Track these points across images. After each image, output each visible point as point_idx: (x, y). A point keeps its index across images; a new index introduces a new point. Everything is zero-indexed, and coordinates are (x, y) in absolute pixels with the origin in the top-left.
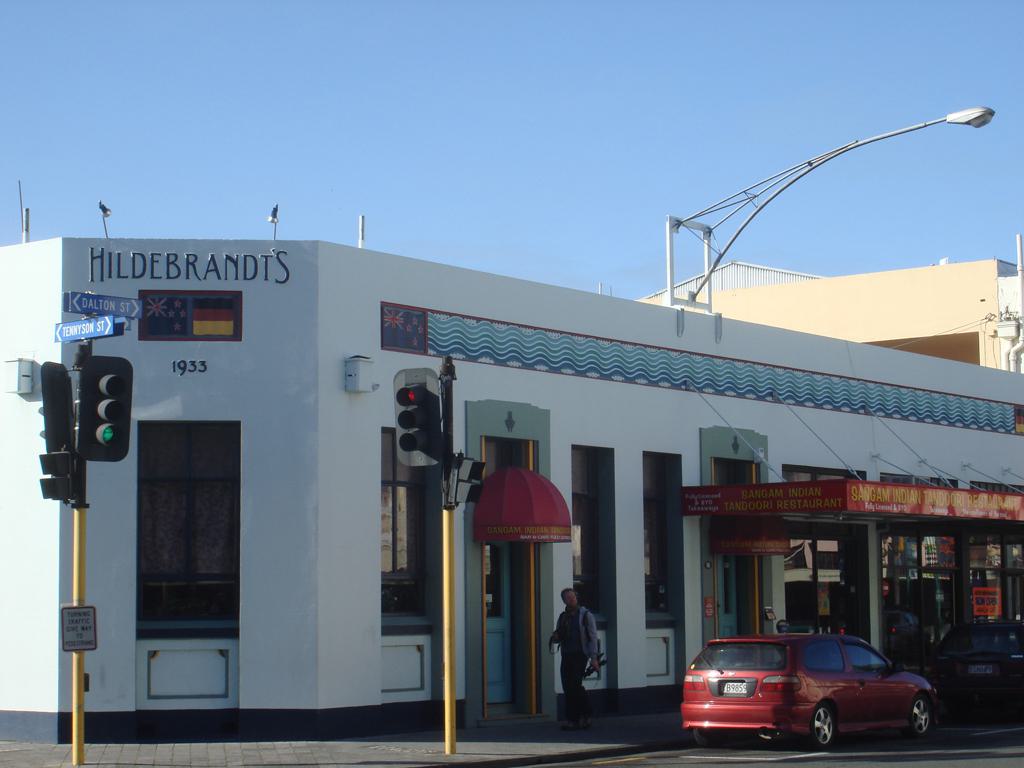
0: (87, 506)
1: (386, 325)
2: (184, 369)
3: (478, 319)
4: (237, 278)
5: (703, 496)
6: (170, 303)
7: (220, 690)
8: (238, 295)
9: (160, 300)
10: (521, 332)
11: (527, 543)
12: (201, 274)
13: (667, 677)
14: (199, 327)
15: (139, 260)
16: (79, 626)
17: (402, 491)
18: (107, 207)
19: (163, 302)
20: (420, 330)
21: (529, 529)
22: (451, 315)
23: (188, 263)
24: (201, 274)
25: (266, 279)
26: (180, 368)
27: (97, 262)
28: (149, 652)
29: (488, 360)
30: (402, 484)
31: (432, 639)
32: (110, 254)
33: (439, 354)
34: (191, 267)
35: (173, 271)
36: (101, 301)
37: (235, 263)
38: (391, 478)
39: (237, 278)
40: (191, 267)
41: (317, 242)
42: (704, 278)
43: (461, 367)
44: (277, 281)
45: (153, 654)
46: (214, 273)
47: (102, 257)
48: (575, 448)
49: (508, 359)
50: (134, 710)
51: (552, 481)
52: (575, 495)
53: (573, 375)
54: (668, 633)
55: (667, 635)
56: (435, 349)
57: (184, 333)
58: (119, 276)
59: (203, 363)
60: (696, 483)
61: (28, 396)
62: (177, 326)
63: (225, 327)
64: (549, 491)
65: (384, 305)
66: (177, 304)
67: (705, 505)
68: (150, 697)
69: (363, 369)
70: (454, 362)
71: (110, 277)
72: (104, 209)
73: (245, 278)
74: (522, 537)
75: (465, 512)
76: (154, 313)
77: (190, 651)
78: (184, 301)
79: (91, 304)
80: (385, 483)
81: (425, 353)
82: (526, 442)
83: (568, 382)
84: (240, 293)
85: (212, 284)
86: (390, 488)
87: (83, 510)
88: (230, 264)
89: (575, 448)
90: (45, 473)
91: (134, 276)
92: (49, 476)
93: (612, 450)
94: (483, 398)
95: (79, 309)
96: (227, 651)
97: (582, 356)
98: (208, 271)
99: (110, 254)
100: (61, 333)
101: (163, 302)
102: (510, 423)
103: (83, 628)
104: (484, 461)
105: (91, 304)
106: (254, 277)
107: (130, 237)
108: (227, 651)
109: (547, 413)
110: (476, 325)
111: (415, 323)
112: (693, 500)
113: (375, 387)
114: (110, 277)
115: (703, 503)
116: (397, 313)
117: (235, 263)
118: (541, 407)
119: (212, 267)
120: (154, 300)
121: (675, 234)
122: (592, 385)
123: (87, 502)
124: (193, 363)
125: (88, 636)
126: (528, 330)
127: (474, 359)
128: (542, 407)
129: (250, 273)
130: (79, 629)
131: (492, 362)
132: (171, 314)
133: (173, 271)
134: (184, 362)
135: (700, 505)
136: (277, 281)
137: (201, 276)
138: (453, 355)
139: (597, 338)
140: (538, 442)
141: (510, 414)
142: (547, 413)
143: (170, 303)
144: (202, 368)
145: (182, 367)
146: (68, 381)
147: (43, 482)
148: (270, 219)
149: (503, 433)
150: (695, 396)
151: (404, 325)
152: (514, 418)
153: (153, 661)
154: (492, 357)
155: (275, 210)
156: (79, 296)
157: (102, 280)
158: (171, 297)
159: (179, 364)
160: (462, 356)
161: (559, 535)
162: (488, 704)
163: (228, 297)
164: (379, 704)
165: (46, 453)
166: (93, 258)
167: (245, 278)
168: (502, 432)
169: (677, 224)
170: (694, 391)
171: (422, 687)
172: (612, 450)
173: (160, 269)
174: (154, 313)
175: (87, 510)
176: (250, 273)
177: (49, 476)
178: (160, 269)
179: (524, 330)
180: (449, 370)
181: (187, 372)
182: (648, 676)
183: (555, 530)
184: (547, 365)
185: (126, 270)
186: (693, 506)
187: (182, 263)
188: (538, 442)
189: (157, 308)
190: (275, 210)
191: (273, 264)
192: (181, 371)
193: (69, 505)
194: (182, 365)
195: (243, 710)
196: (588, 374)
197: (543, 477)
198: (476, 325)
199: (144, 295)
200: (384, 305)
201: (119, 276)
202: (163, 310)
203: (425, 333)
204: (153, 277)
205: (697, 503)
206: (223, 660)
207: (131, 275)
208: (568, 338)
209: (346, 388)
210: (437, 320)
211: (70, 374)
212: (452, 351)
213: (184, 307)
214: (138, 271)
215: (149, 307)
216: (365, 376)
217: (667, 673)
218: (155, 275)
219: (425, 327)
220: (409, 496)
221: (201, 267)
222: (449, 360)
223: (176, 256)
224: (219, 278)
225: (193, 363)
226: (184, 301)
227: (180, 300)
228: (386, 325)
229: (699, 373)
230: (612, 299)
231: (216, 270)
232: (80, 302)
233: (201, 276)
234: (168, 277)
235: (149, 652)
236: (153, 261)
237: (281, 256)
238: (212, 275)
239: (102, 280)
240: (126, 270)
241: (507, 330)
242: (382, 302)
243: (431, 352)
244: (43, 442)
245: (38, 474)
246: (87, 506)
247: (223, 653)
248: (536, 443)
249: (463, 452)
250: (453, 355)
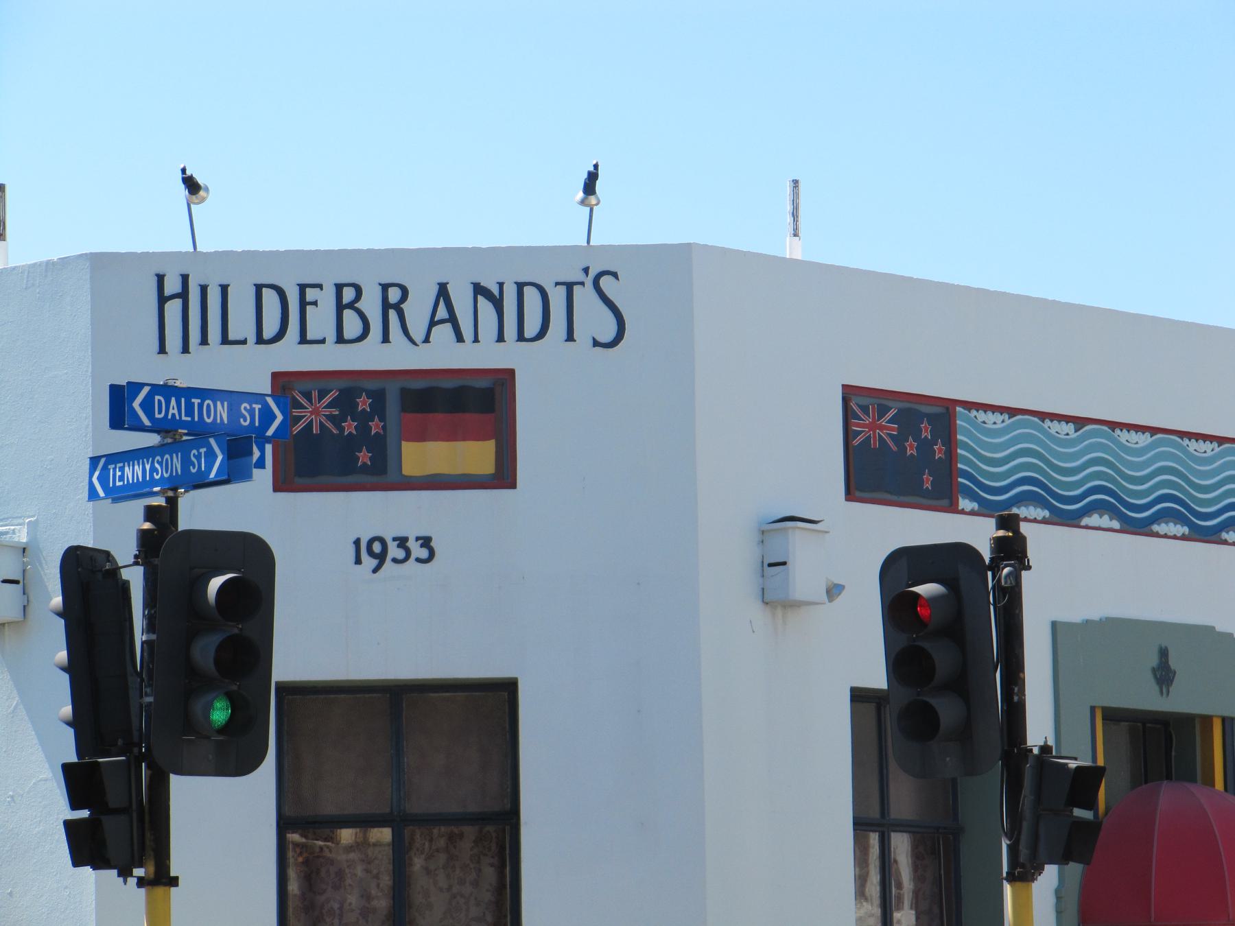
0: (174, 882)
2: (381, 558)
3: (1079, 422)
4: (501, 338)
10: (1185, 450)
17: (901, 844)
18: (200, 180)
19: (328, 399)
20: (939, 451)
22: (1012, 412)
23: (386, 306)
24: (418, 332)
25: (570, 337)
26: (371, 553)
27: (173, 309)
29: (1105, 521)
30: (901, 826)
32: (204, 289)
33: (985, 509)
34: (393, 315)
35: (352, 325)
36: (196, 401)
38: (874, 813)
40: (393, 315)
44: (596, 343)
46: (448, 327)
47: (184, 295)
49: (1156, 518)
56: (973, 497)
58: (225, 340)
59: (426, 542)
61: (911, 908)
62: (364, 457)
65: (849, 392)
66: (364, 403)
70: (1024, 528)
71: (204, 341)
72: (192, 185)
73: (521, 337)
78: (378, 397)
79: (173, 410)
80: (861, 825)
81: (953, 508)
82: (1207, 720)
84: (511, 373)
86: (874, 839)
87: (160, 891)
88: (485, 305)
90: (74, 805)
91: (260, 340)
92: (84, 814)
94: (1095, 614)
95: (147, 422)
99: (204, 289)
100: (103, 480)
101: (328, 399)
102: (1164, 675)
104: (1101, 762)
105: (173, 410)
106: (541, 334)
107: (609, 244)
110: (1073, 435)
111: (926, 434)
113: (833, 591)
114: (204, 341)
116: (883, 411)
117: (498, 304)
119: (442, 313)
120: (307, 396)
124: (402, 542)
126: (1134, 437)
127: (1070, 520)
129: (532, 325)
131: (1116, 524)
132: (350, 427)
133: (352, 325)
136: (596, 343)
138: (1022, 511)
141: (1164, 653)
144: (424, 553)
146: (125, 587)
147: (69, 825)
148: (581, 195)
149: (1148, 699)
151: (899, 440)
152: (1173, 663)
154: (1115, 513)
156: (146, 390)
157: (185, 349)
163: (482, 383)
165: (73, 758)
167: (521, 337)
173: (321, 320)
175: (173, 889)
176: (532, 325)
177: (84, 814)
178: (321, 320)
179: (1193, 445)
181: (388, 562)
185: (241, 325)
187: (371, 304)
189: (315, 415)
191: (585, 297)
192: (374, 562)
193: (132, 881)
196: (1155, 528)
198: (1073, 435)
199: (283, 382)
200: (849, 392)
201: (225, 340)
202: (330, 418)
204: (303, 340)
207: (252, 338)
210: (982, 428)
211: (125, 574)
212: (1021, 499)
213: (379, 407)
214: (271, 326)
215: (296, 412)
218: (231, 337)
220: (918, 856)
221: (418, 311)
222: (1008, 522)
224: (460, 338)
225: (402, 542)
227: (370, 394)
228: (856, 442)
231: (452, 319)
234: (340, 339)
236: (303, 304)
237: (605, 282)
238: (443, 332)
239: (185, 349)
240: (241, 325)
242: (846, 387)
243: (965, 504)
246: (174, 882)
249: (1051, 742)
250: (1022, 511)
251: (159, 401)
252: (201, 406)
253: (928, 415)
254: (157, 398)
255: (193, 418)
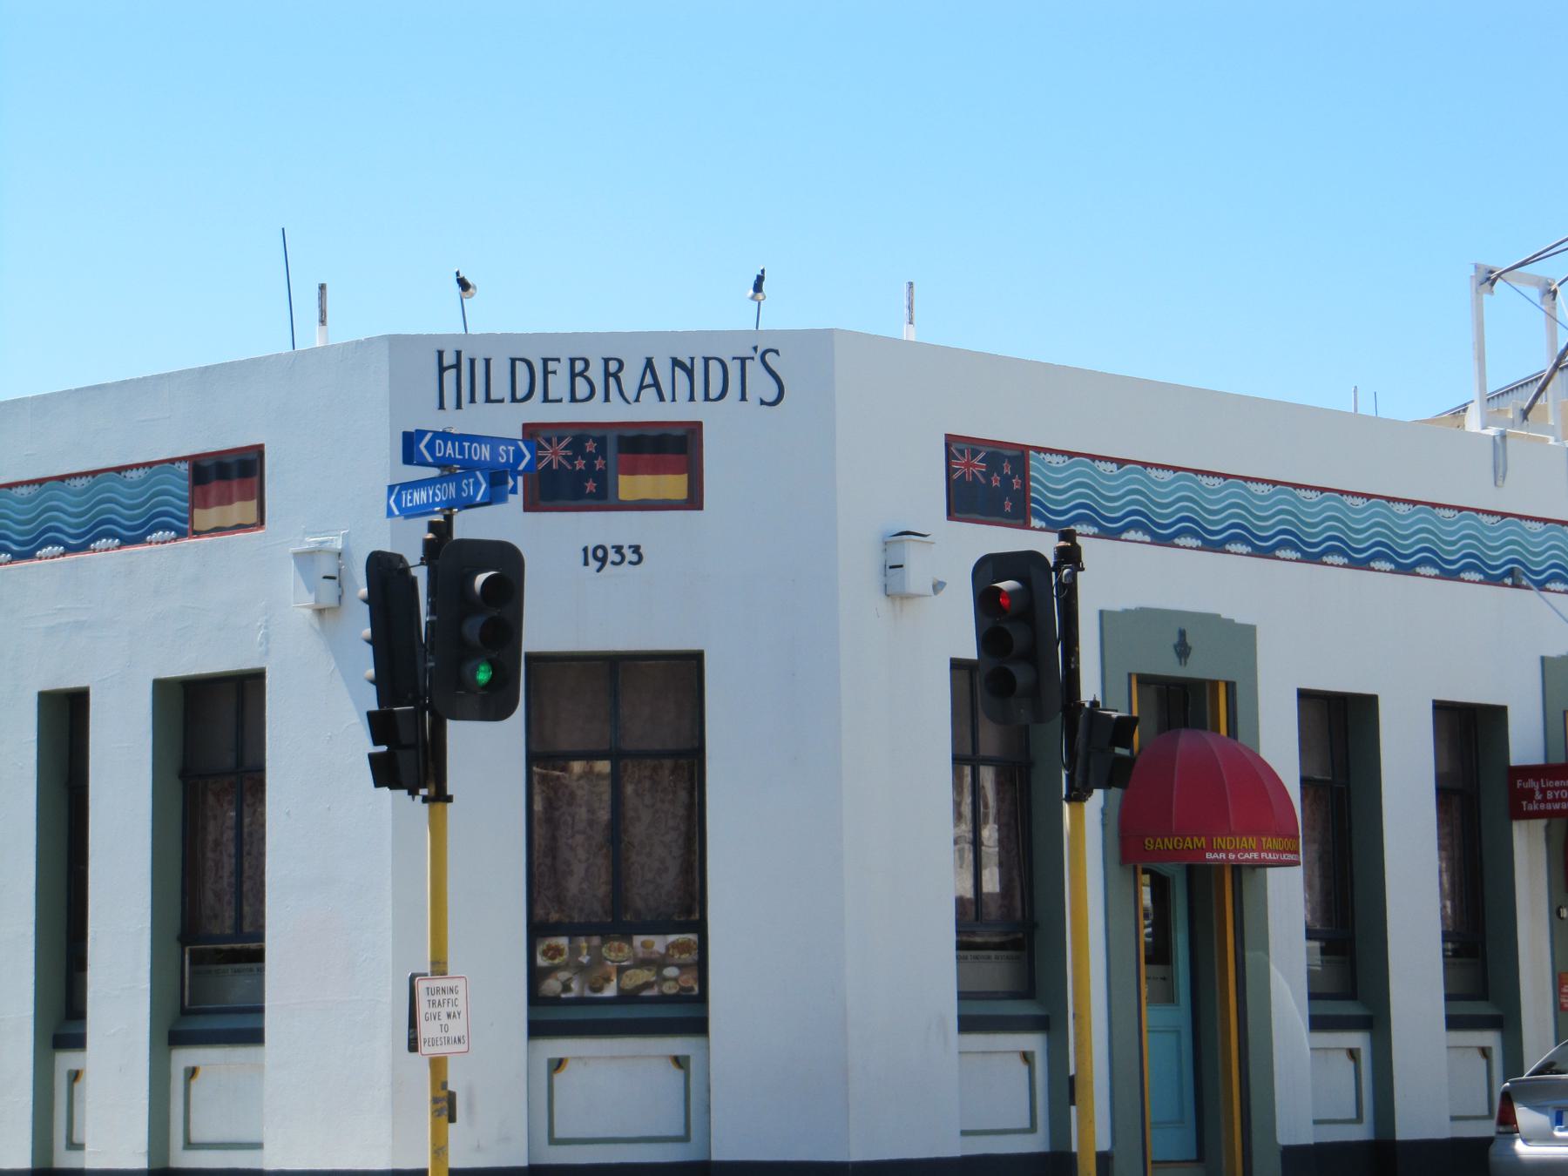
0: (449, 799)
1: (955, 476)
2: (603, 561)
3: (1121, 462)
4: (692, 398)
5: (1550, 784)
6: (577, 445)
7: (677, 1129)
8: (695, 428)
9: (560, 440)
10: (1248, 490)
11: (1220, 867)
12: (630, 392)
13: (1029, 1137)
14: (630, 486)
15: (521, 369)
16: (444, 1011)
17: (987, 775)
18: (470, 280)
20: (1016, 483)
21: (1219, 841)
22: (1071, 455)
23: (607, 374)
24: (630, 392)
25: (743, 398)
26: (595, 557)
27: (450, 376)
28: (550, 1061)
29: (1139, 536)
30: (988, 761)
31: (1048, 1038)
32: (472, 362)
33: (1051, 526)
34: (612, 381)
35: (582, 389)
36: (466, 444)
37: (690, 373)
38: (968, 751)
39: (692, 398)
40: (612, 381)
41: (829, 333)
42: (1540, 382)
43: (1092, 549)
44: (762, 402)
45: (557, 1065)
46: (653, 390)
48: (1304, 696)
50: (522, 1162)
51: (1263, 754)
52: (1305, 782)
53: (1344, 566)
54: (1358, 1040)
55: (1485, 1044)
57: (602, 498)
58: (488, 400)
59: (636, 549)
60: (1538, 759)
62: (590, 486)
63: (673, 485)
64: (1261, 778)
65: (950, 440)
66: (590, 447)
67: (1554, 800)
68: (553, 1141)
69: (912, 553)
70: (1080, 540)
71: (472, 400)
72: (464, 285)
73: (707, 398)
74: (1209, 856)
75: (1104, 812)
76: (551, 462)
77: (613, 1058)
78: (601, 442)
79: (449, 451)
80: (958, 760)
83: (1287, 573)
84: (699, 425)
85: (649, 410)
86: (967, 770)
87: (439, 805)
89: (1304, 696)
90: (376, 742)
91: (514, 399)
92: (384, 748)
93: (1372, 700)
96: (687, 1058)
97: (1314, 525)
98: (642, 387)
102: (1183, 650)
103: (449, 1016)
104: (1135, 714)
105: (449, 451)
108: (687, 1058)
109: (1249, 632)
112: (1532, 791)
113: (938, 587)
114: (472, 400)
115: (1550, 795)
116: (975, 453)
117: (690, 373)
118: (1238, 620)
119: (648, 379)
120: (549, 441)
121: (1486, 297)
122: (1334, 578)
123: (449, 792)
124: (619, 549)
125: (72, 1029)
126: (1212, 481)
127: (1114, 535)
128: (1240, 619)
129: (715, 391)
130: (444, 1016)
131: (1147, 538)
132: (580, 464)
133: (582, 389)
134: (603, 548)
135: (1545, 800)
136: (762, 402)
137: (631, 395)
138: (1078, 529)
139: (1342, 493)
140: (1234, 684)
141: (1182, 634)
142: (1249, 632)
143: (577, 445)
144: (635, 558)
145: (598, 556)
146: (413, 582)
147: (372, 757)
148: (751, 292)
150: (1531, 597)
151: (987, 475)
153: (557, 1077)
154: (1147, 531)
155: (760, 280)
156: (429, 436)
157: (459, 406)
158: (580, 436)
159: (595, 550)
160: (1093, 530)
161: (1278, 851)
162: (1153, 1162)
163: (679, 432)
164: (959, 1155)
166: (442, 369)
167: (707, 398)
168: (1167, 666)
169: (1489, 279)
170: (1527, 588)
171: (1032, 1129)
172: (1372, 700)
174: (551, 462)
175: (449, 805)
176: (715, 391)
177: (384, 748)
180: (1070, 556)
181: (608, 565)
182: (964, 1133)
183: (1268, 842)
184: (1249, 543)
185: (500, 388)
186: (1531, 799)
187: (596, 373)
188: (1234, 684)
189: (554, 455)
190: (760, 280)
191: (754, 368)
192: (598, 564)
193: (418, 799)
194: (600, 553)
195: (714, 1162)
197: (1246, 749)
198: (1116, 472)
199: (530, 430)
200: (950, 440)
201: (488, 400)
202: (565, 457)
203: (1025, 487)
204: (546, 399)
205: (1538, 796)
206: (680, 1074)
208: (1086, 465)
209: (887, 593)
211: (414, 572)
214: (521, 391)
215: (540, 453)
216: (920, 567)
217: (1032, 1129)
219: (1025, 478)
221: (630, 379)
222: (1068, 535)
223: (587, 362)
224: (662, 398)
226: (601, 442)
228: (955, 476)
229: (1405, 538)
230: (1375, 423)
231: (656, 384)
232: (430, 447)
233: (631, 395)
235: (550, 1061)
236: (546, 373)
237: (769, 357)
238: (650, 393)
239: (459, 406)
240: (500, 388)
241: (1226, 487)
243: (1035, 522)
244: (372, 691)
245: (364, 745)
246: (449, 799)
247: (680, 1062)
248: (1231, 687)
249: (1099, 699)
250: (1078, 529)
251: (439, 444)
252: (470, 448)
253: (1009, 457)
254: (438, 441)
255: (464, 456)
